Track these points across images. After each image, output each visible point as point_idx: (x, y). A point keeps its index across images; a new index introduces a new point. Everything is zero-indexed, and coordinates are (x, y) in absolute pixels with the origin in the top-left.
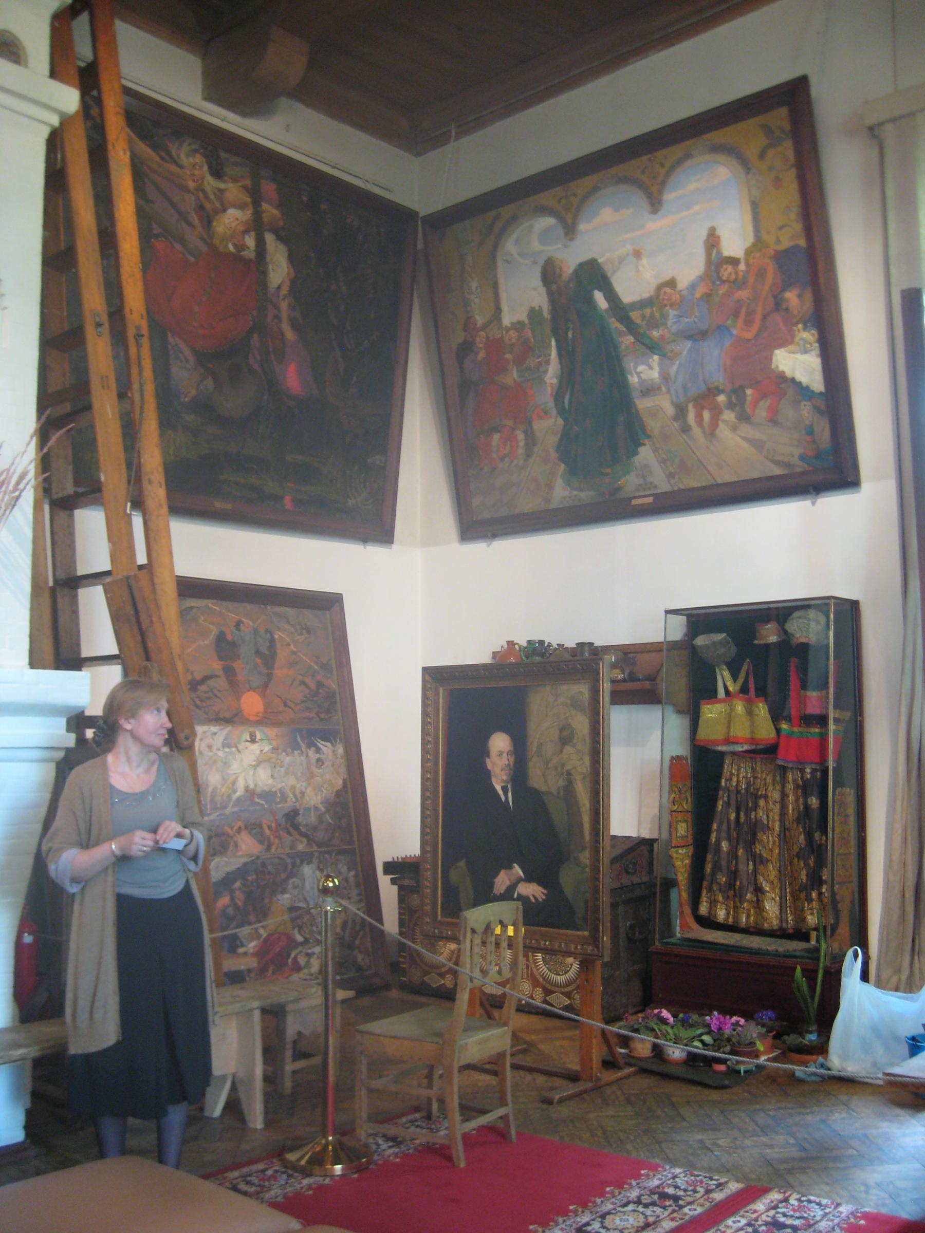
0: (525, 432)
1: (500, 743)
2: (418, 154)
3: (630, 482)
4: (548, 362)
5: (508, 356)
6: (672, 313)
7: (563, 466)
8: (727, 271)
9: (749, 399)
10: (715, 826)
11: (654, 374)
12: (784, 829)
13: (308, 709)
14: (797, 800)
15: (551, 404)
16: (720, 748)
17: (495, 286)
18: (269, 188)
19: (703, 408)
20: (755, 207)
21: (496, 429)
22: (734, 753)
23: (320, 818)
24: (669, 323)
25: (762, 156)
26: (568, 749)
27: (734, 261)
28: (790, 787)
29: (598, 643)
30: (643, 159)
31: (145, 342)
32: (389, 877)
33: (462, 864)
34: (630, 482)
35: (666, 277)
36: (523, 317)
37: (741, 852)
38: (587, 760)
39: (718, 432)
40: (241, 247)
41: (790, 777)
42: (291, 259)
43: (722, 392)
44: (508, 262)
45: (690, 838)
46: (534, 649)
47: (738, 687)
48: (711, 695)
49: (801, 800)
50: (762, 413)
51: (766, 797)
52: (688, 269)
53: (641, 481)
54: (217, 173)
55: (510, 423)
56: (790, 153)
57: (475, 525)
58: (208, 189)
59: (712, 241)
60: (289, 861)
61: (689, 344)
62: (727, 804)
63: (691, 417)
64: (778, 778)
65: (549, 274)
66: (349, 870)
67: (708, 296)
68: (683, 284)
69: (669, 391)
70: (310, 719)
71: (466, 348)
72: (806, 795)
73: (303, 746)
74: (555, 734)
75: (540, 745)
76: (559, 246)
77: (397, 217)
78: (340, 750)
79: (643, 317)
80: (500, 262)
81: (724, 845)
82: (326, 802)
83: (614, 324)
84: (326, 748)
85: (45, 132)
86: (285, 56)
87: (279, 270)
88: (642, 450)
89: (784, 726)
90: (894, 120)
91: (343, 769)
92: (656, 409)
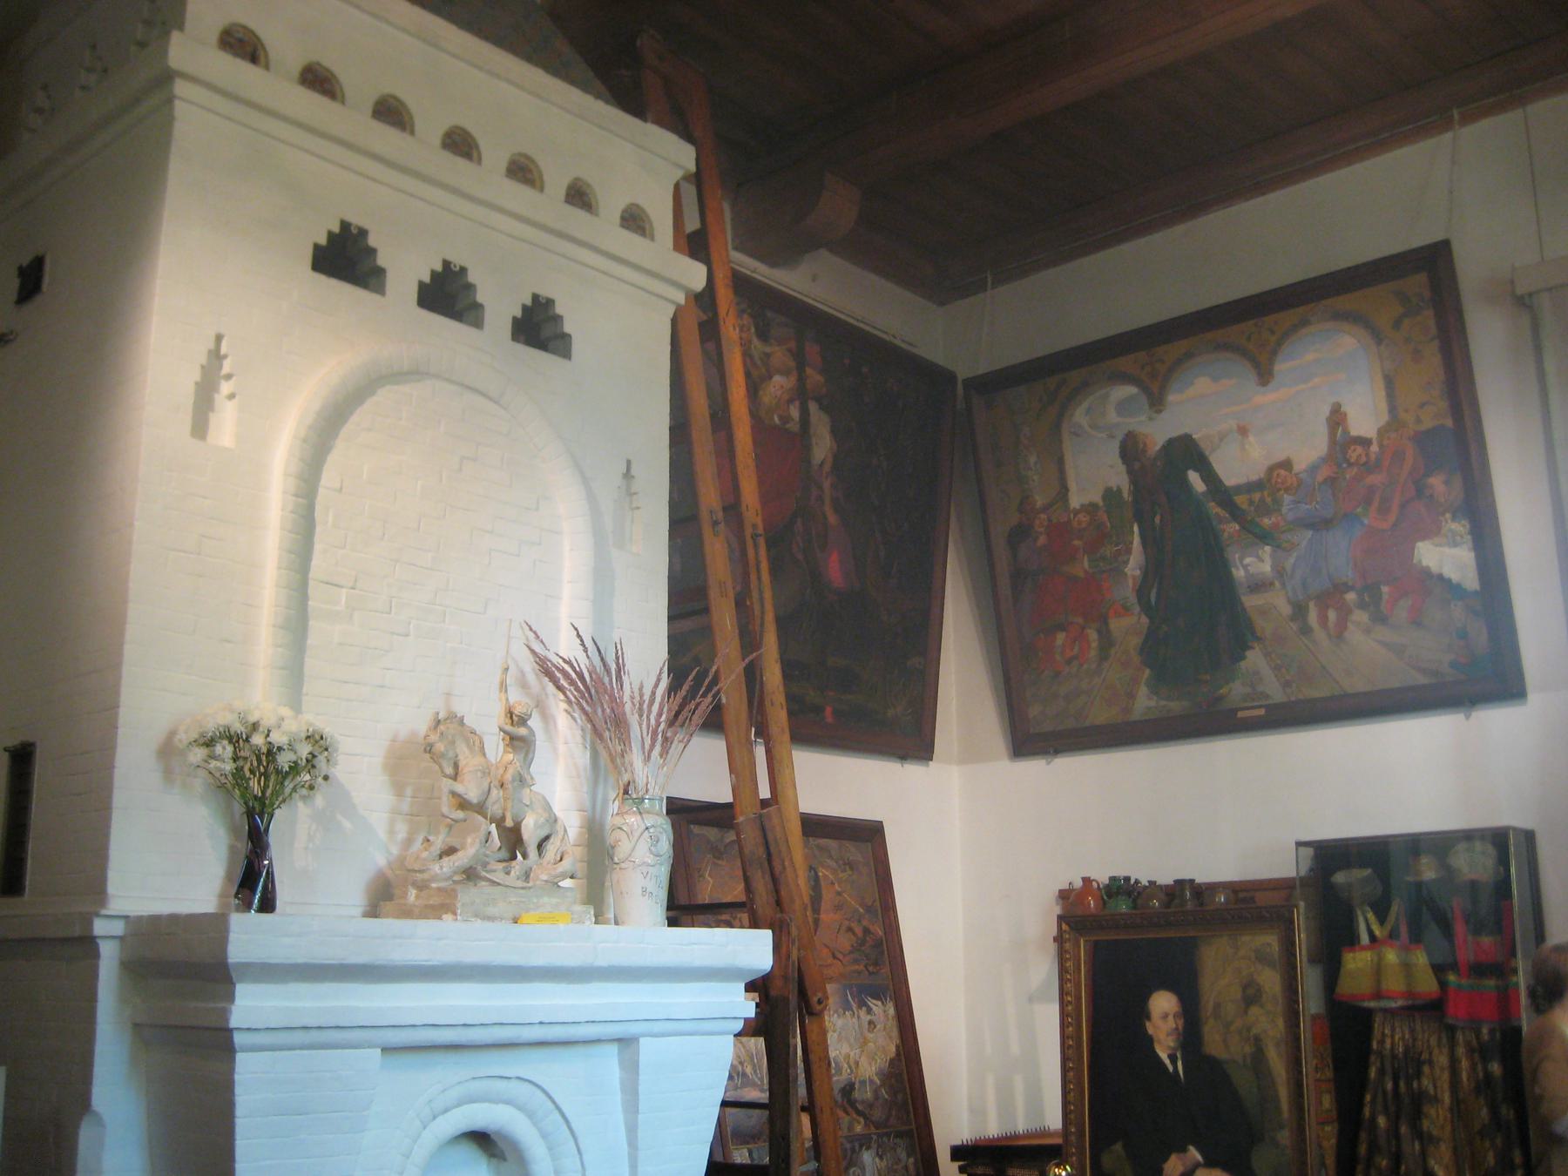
0: (1099, 632)
1: (1163, 1004)
2: (942, 304)
3: (1236, 691)
4: (1129, 551)
5: (1076, 542)
6: (1287, 498)
7: (1148, 671)
8: (1355, 453)
9: (1385, 597)
10: (1368, 1098)
11: (1266, 568)
12: (1457, 1101)
13: (856, 961)
14: (1473, 1067)
15: (1132, 598)
16: (1366, 1004)
17: (1061, 462)
18: (813, 350)
19: (1327, 607)
20: (1390, 383)
21: (1062, 627)
22: (1385, 1011)
23: (876, 1092)
24: (1284, 510)
25: (1397, 324)
26: (1255, 1011)
27: (1365, 442)
28: (1461, 1051)
29: (1201, 878)
30: (1251, 324)
31: (762, 542)
32: (956, 1165)
33: (1118, 1147)
34: (1236, 691)
35: (1280, 456)
36: (1096, 497)
37: (1403, 1129)
38: (1280, 1023)
39: (1346, 634)
40: (786, 419)
41: (1460, 1037)
42: (834, 432)
43: (1352, 588)
44: (1077, 435)
45: (1334, 1113)
46: (1119, 887)
47: (1386, 932)
48: (1352, 941)
49: (1480, 1067)
50: (1402, 611)
51: (1430, 1062)
52: (1307, 448)
53: (1249, 690)
54: (763, 336)
55: (1080, 620)
56: (1432, 323)
57: (1028, 740)
58: (756, 355)
59: (1337, 418)
60: (848, 1146)
61: (1309, 533)
62: (1381, 1072)
63: (1313, 617)
64: (1444, 1040)
65: (1130, 449)
66: (909, 1156)
67: (1331, 481)
68: (1300, 465)
69: (1283, 585)
70: (859, 973)
71: (1020, 534)
72: (1485, 1060)
73: (854, 1006)
74: (1236, 992)
75: (1217, 1006)
76: (1143, 418)
77: (935, 378)
78: (892, 1011)
79: (1251, 502)
80: (1066, 436)
81: (1382, 1121)
82: (880, 1073)
83: (1214, 509)
84: (876, 1006)
85: (671, 310)
86: (839, 204)
87: (823, 447)
88: (1249, 654)
89: (1452, 978)
90: (1550, 289)
91: (895, 1033)
92: (1269, 608)
